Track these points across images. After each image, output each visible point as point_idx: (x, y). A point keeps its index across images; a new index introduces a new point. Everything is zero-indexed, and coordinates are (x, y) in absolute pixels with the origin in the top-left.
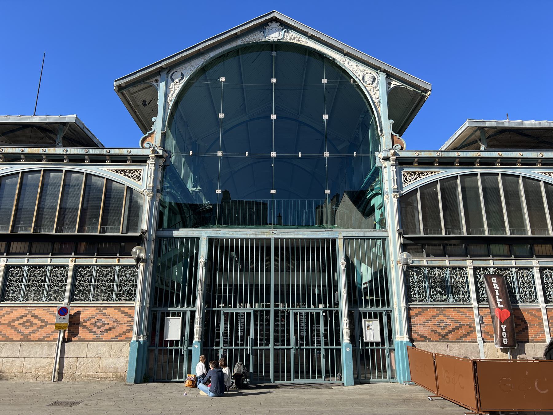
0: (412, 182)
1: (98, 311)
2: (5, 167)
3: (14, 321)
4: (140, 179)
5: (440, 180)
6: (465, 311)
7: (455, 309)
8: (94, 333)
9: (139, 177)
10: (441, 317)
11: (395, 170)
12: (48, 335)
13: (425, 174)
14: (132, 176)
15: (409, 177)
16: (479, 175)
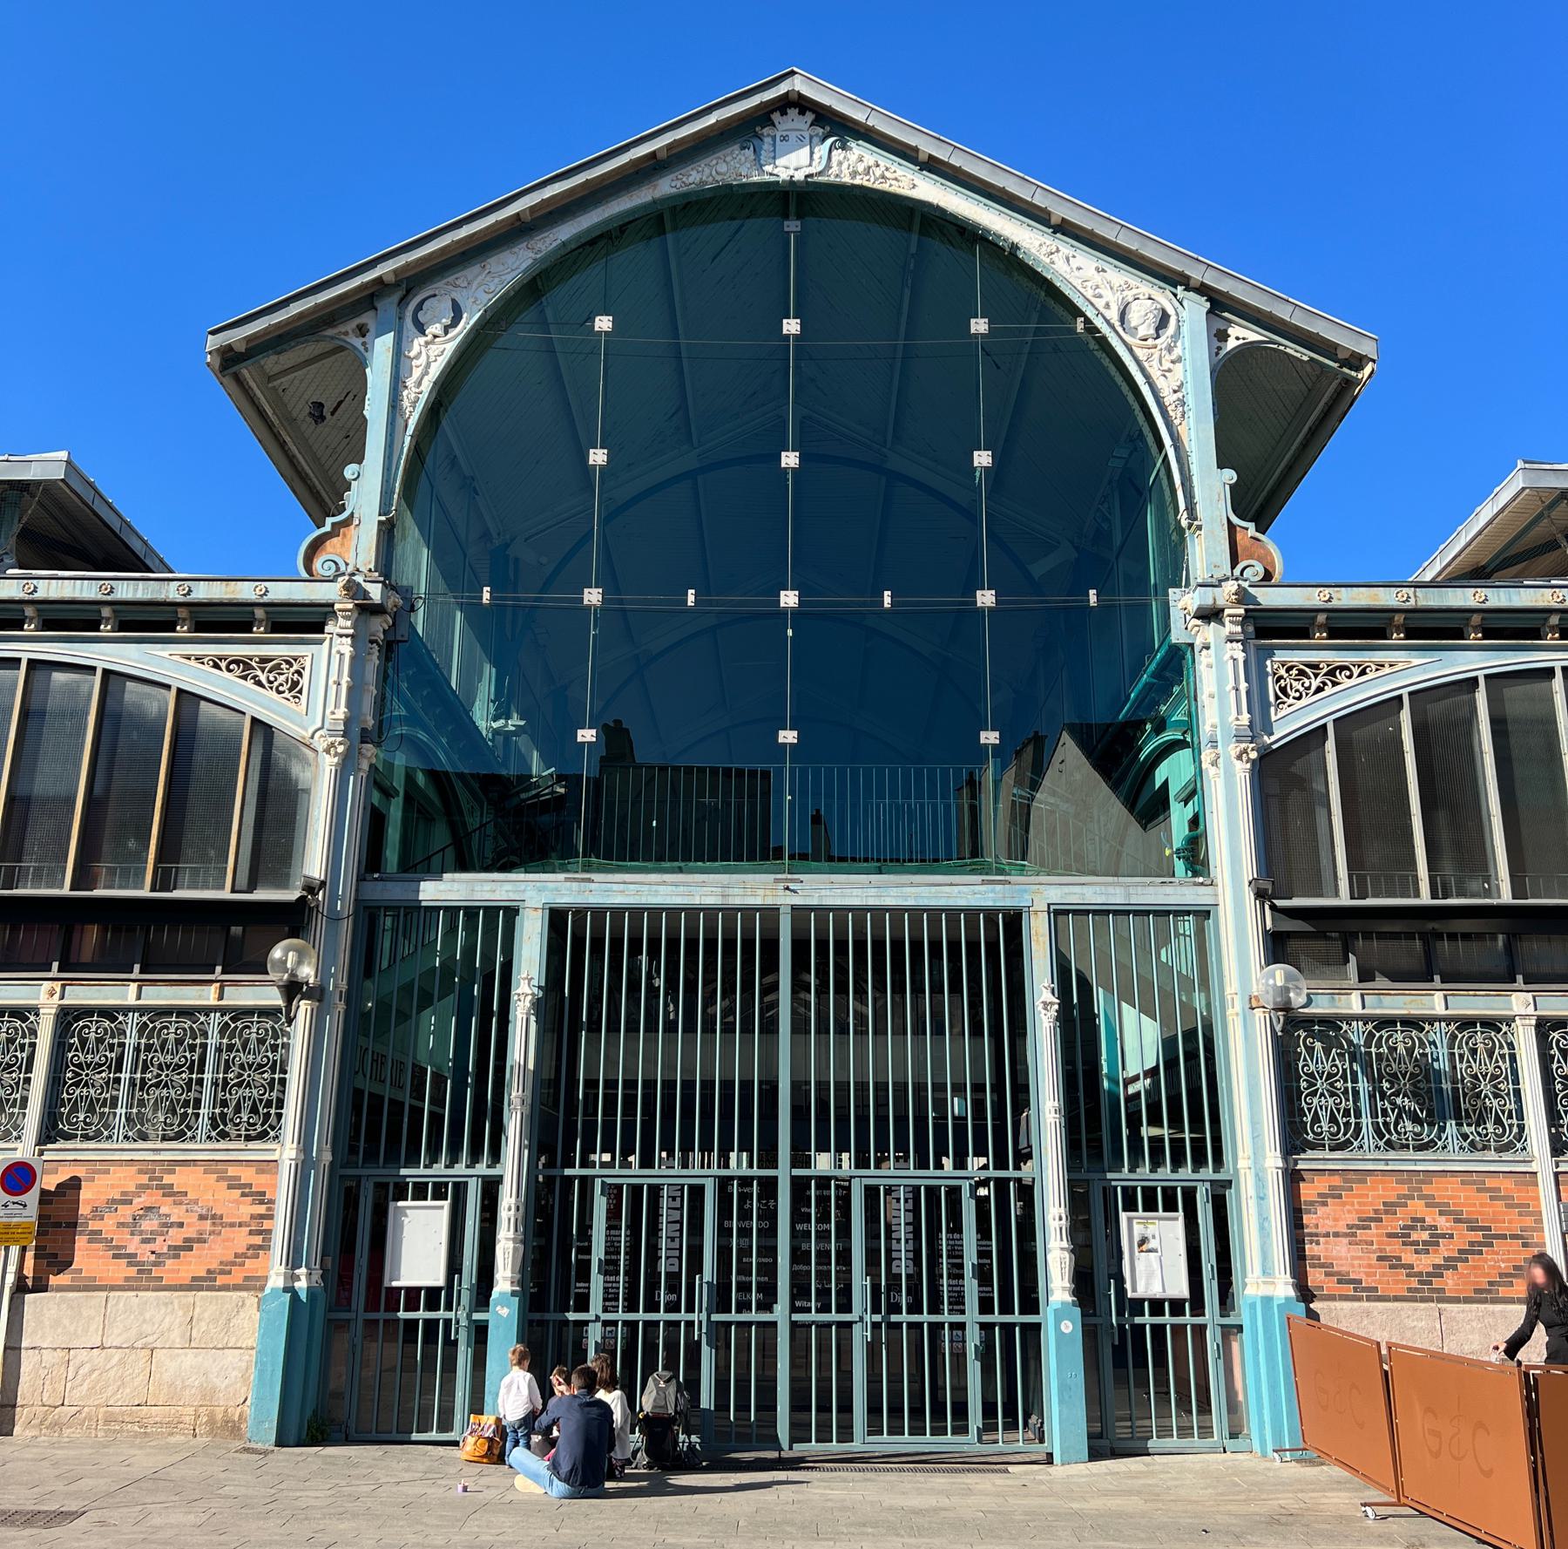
0: (1304, 702)
1: (144, 1179)
2: (1417, 659)
4: (300, 692)
5: (1410, 694)
6: (1506, 1185)
8: (131, 1258)
9: (295, 684)
10: (1417, 1207)
11: (1241, 656)
13: (1356, 671)
14: (272, 679)
15: (1295, 684)
16: (1559, 674)
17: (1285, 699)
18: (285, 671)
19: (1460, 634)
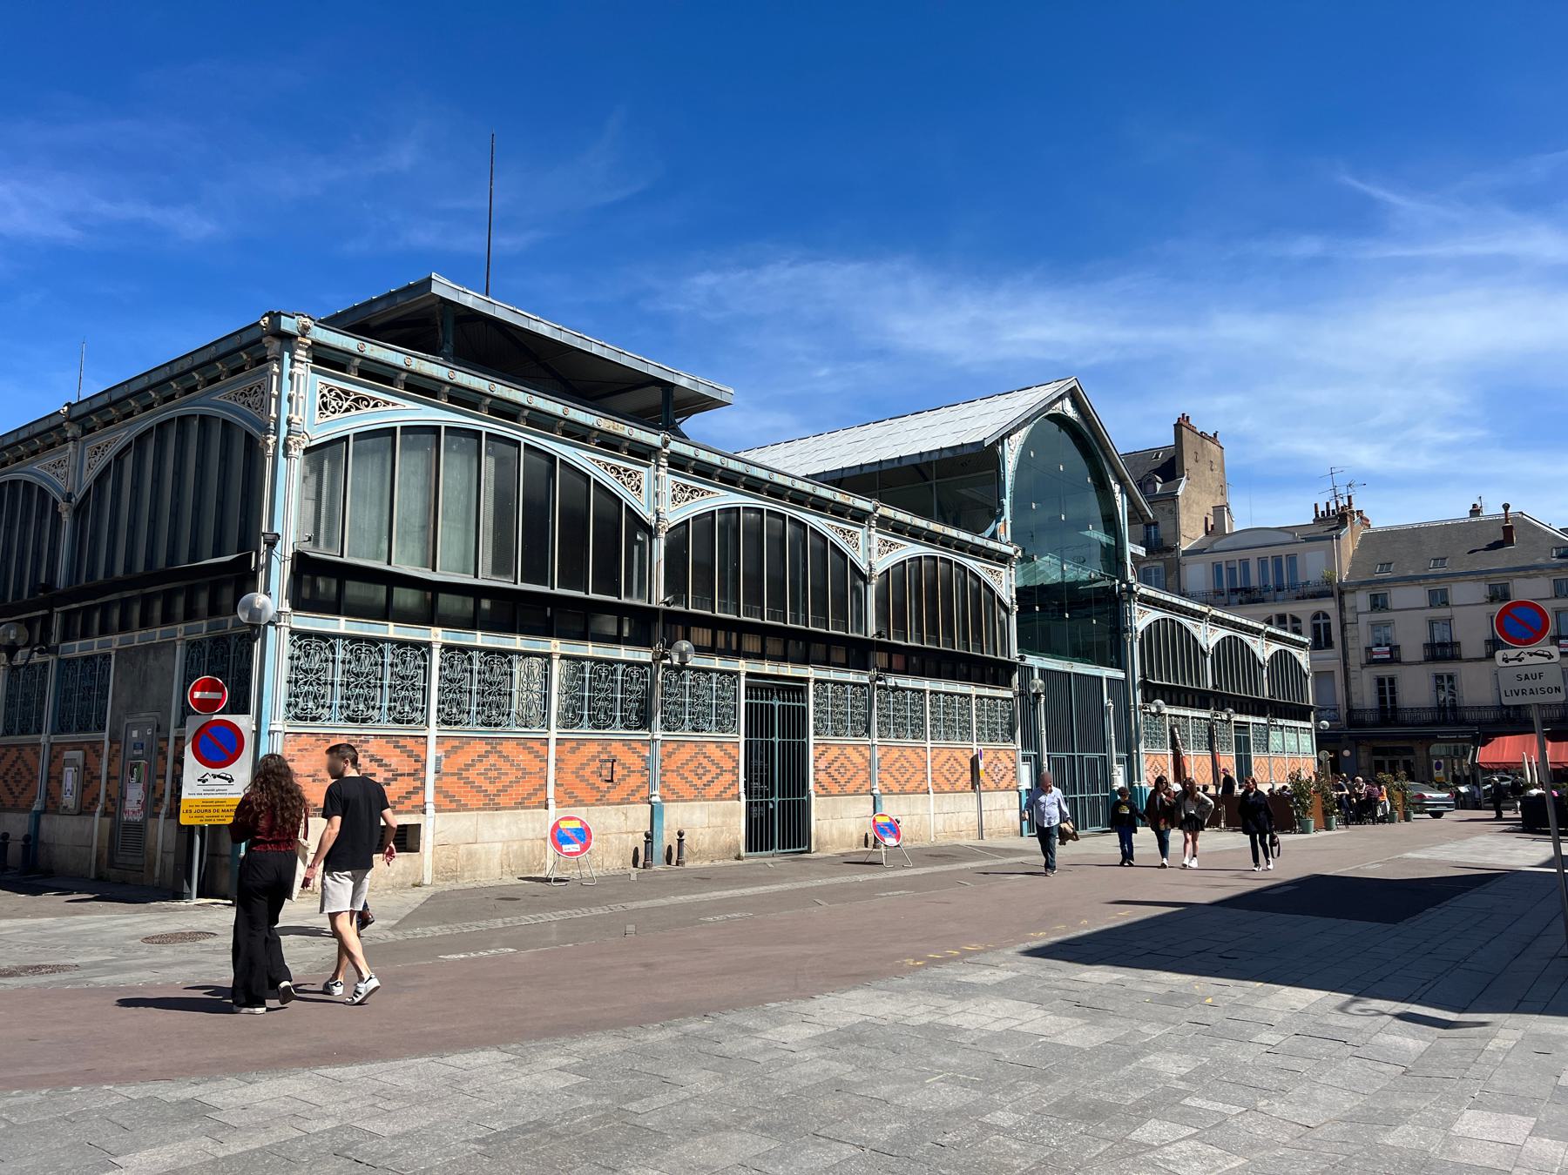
0: (337, 415)
1: (489, 748)
3: (468, 767)
4: (640, 492)
5: (402, 427)
6: (410, 743)
7: (519, 741)
9: (638, 487)
12: (633, 793)
13: (372, 403)
15: (333, 402)
17: (324, 411)
18: (328, 400)
19: (434, 394)
